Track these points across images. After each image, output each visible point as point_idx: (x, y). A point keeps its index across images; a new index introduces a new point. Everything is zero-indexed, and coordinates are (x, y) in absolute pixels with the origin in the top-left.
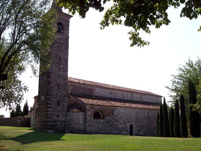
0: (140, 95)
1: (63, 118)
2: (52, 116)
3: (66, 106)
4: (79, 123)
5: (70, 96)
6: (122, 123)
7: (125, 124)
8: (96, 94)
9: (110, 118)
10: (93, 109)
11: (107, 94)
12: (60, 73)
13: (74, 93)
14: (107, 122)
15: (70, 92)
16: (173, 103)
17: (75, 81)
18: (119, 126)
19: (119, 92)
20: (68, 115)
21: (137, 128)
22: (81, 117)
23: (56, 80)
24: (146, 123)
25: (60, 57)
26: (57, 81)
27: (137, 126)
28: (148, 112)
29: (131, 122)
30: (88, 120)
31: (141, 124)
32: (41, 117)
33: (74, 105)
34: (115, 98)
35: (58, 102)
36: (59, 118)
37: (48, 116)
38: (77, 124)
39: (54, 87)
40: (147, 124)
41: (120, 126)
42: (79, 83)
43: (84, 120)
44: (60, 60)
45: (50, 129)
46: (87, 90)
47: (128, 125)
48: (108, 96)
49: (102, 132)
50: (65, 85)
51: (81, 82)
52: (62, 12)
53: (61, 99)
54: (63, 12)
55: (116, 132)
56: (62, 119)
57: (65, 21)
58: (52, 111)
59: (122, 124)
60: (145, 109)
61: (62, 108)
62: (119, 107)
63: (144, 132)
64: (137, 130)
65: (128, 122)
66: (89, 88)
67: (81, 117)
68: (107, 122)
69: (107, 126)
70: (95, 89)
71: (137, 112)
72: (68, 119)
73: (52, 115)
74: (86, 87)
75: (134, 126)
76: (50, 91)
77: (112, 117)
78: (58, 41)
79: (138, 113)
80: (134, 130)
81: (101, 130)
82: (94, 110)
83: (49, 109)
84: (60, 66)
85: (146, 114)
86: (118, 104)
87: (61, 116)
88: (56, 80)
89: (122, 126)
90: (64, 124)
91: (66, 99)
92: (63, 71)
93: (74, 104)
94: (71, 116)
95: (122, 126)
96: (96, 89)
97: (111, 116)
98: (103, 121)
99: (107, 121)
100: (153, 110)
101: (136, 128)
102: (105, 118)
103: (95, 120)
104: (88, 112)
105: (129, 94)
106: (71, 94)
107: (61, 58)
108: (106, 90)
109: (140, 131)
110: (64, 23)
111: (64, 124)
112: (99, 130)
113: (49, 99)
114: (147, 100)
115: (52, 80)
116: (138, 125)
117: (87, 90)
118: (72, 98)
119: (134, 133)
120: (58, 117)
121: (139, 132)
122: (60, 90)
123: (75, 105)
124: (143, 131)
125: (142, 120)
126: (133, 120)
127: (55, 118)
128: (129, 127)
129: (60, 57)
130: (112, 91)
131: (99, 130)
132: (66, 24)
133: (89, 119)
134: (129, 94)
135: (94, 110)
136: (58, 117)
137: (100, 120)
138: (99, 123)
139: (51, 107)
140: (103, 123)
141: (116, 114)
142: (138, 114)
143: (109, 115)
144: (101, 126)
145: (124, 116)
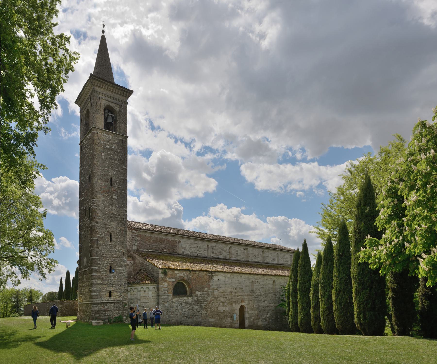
0: (261, 250)
1: (120, 297)
2: (100, 295)
3: (125, 274)
4: (147, 304)
5: (135, 255)
6: (226, 304)
7: (231, 304)
8: (182, 251)
9: (203, 294)
10: (173, 278)
11: (200, 250)
12: (113, 212)
13: (142, 250)
14: (198, 302)
15: (135, 248)
16: (96, 271)
17: (146, 227)
18: (219, 309)
19: (224, 245)
20: (129, 290)
21: (253, 312)
22: (150, 293)
23: (106, 225)
24: (270, 303)
25: (111, 179)
26: (107, 226)
27: (252, 309)
28: (274, 282)
29: (243, 301)
30: (164, 299)
31: (260, 304)
32: (83, 297)
33: (142, 272)
34: (216, 256)
35: (111, 267)
36: (112, 298)
37: (93, 294)
38: (143, 306)
39: (102, 238)
40: (271, 305)
41: (222, 309)
42: (151, 230)
43: (157, 300)
44: (111, 185)
45: (96, 319)
46: (165, 242)
47: (237, 307)
48: (204, 253)
49: (189, 321)
50: (121, 234)
51: (155, 229)
52: (114, 84)
53: (117, 260)
54: (116, 82)
55: (213, 320)
56: (119, 299)
57: (119, 103)
58: (99, 284)
59: (224, 306)
60: (268, 277)
61: (118, 278)
62: (220, 274)
63: (266, 321)
64: (253, 316)
65: (237, 302)
66: (168, 240)
67: (150, 293)
68: (198, 302)
69: (198, 310)
70: (180, 242)
71: (253, 281)
72: (129, 298)
73: (99, 291)
74: (164, 238)
75: (247, 310)
76: (95, 246)
77: (206, 291)
78: (108, 147)
79: (254, 283)
80: (247, 316)
81: (187, 317)
82: (174, 280)
83: (94, 281)
84: (112, 197)
85: (271, 286)
86: (219, 268)
87: (116, 294)
88: (106, 225)
89: (224, 309)
90: (121, 308)
91: (124, 261)
92: (119, 207)
93: (141, 269)
94: (133, 292)
95: (224, 309)
96: (182, 240)
97: (206, 289)
98: (190, 300)
99: (198, 300)
100: (283, 278)
101: (250, 312)
102: (194, 295)
103: (176, 299)
104: (163, 284)
105: (240, 250)
106: (137, 252)
107: (113, 180)
108: (200, 242)
109: (258, 319)
110: (117, 108)
111: (121, 308)
112: (183, 317)
113: (93, 261)
114: (68, 190)
115: (110, 229)
116: (255, 306)
117: (165, 242)
118: (139, 259)
119: (247, 323)
120: (110, 295)
121: (256, 319)
122: (114, 243)
123: (142, 271)
124: (264, 317)
125: (262, 298)
126: (246, 297)
127: (106, 298)
128: (237, 311)
129: (111, 179)
130: (211, 245)
131: (183, 317)
132: (120, 110)
133: (165, 297)
134: (240, 250)
135: (174, 280)
136: (110, 295)
137: (184, 298)
138: (184, 304)
139: (99, 278)
140: (191, 304)
141: (215, 287)
142: (255, 286)
143: (202, 290)
144: (187, 309)
145: (228, 291)
